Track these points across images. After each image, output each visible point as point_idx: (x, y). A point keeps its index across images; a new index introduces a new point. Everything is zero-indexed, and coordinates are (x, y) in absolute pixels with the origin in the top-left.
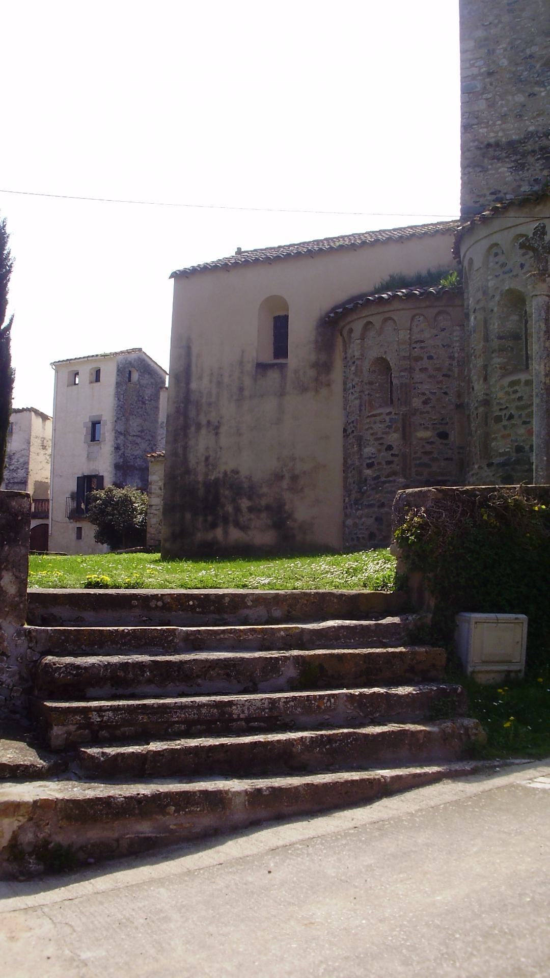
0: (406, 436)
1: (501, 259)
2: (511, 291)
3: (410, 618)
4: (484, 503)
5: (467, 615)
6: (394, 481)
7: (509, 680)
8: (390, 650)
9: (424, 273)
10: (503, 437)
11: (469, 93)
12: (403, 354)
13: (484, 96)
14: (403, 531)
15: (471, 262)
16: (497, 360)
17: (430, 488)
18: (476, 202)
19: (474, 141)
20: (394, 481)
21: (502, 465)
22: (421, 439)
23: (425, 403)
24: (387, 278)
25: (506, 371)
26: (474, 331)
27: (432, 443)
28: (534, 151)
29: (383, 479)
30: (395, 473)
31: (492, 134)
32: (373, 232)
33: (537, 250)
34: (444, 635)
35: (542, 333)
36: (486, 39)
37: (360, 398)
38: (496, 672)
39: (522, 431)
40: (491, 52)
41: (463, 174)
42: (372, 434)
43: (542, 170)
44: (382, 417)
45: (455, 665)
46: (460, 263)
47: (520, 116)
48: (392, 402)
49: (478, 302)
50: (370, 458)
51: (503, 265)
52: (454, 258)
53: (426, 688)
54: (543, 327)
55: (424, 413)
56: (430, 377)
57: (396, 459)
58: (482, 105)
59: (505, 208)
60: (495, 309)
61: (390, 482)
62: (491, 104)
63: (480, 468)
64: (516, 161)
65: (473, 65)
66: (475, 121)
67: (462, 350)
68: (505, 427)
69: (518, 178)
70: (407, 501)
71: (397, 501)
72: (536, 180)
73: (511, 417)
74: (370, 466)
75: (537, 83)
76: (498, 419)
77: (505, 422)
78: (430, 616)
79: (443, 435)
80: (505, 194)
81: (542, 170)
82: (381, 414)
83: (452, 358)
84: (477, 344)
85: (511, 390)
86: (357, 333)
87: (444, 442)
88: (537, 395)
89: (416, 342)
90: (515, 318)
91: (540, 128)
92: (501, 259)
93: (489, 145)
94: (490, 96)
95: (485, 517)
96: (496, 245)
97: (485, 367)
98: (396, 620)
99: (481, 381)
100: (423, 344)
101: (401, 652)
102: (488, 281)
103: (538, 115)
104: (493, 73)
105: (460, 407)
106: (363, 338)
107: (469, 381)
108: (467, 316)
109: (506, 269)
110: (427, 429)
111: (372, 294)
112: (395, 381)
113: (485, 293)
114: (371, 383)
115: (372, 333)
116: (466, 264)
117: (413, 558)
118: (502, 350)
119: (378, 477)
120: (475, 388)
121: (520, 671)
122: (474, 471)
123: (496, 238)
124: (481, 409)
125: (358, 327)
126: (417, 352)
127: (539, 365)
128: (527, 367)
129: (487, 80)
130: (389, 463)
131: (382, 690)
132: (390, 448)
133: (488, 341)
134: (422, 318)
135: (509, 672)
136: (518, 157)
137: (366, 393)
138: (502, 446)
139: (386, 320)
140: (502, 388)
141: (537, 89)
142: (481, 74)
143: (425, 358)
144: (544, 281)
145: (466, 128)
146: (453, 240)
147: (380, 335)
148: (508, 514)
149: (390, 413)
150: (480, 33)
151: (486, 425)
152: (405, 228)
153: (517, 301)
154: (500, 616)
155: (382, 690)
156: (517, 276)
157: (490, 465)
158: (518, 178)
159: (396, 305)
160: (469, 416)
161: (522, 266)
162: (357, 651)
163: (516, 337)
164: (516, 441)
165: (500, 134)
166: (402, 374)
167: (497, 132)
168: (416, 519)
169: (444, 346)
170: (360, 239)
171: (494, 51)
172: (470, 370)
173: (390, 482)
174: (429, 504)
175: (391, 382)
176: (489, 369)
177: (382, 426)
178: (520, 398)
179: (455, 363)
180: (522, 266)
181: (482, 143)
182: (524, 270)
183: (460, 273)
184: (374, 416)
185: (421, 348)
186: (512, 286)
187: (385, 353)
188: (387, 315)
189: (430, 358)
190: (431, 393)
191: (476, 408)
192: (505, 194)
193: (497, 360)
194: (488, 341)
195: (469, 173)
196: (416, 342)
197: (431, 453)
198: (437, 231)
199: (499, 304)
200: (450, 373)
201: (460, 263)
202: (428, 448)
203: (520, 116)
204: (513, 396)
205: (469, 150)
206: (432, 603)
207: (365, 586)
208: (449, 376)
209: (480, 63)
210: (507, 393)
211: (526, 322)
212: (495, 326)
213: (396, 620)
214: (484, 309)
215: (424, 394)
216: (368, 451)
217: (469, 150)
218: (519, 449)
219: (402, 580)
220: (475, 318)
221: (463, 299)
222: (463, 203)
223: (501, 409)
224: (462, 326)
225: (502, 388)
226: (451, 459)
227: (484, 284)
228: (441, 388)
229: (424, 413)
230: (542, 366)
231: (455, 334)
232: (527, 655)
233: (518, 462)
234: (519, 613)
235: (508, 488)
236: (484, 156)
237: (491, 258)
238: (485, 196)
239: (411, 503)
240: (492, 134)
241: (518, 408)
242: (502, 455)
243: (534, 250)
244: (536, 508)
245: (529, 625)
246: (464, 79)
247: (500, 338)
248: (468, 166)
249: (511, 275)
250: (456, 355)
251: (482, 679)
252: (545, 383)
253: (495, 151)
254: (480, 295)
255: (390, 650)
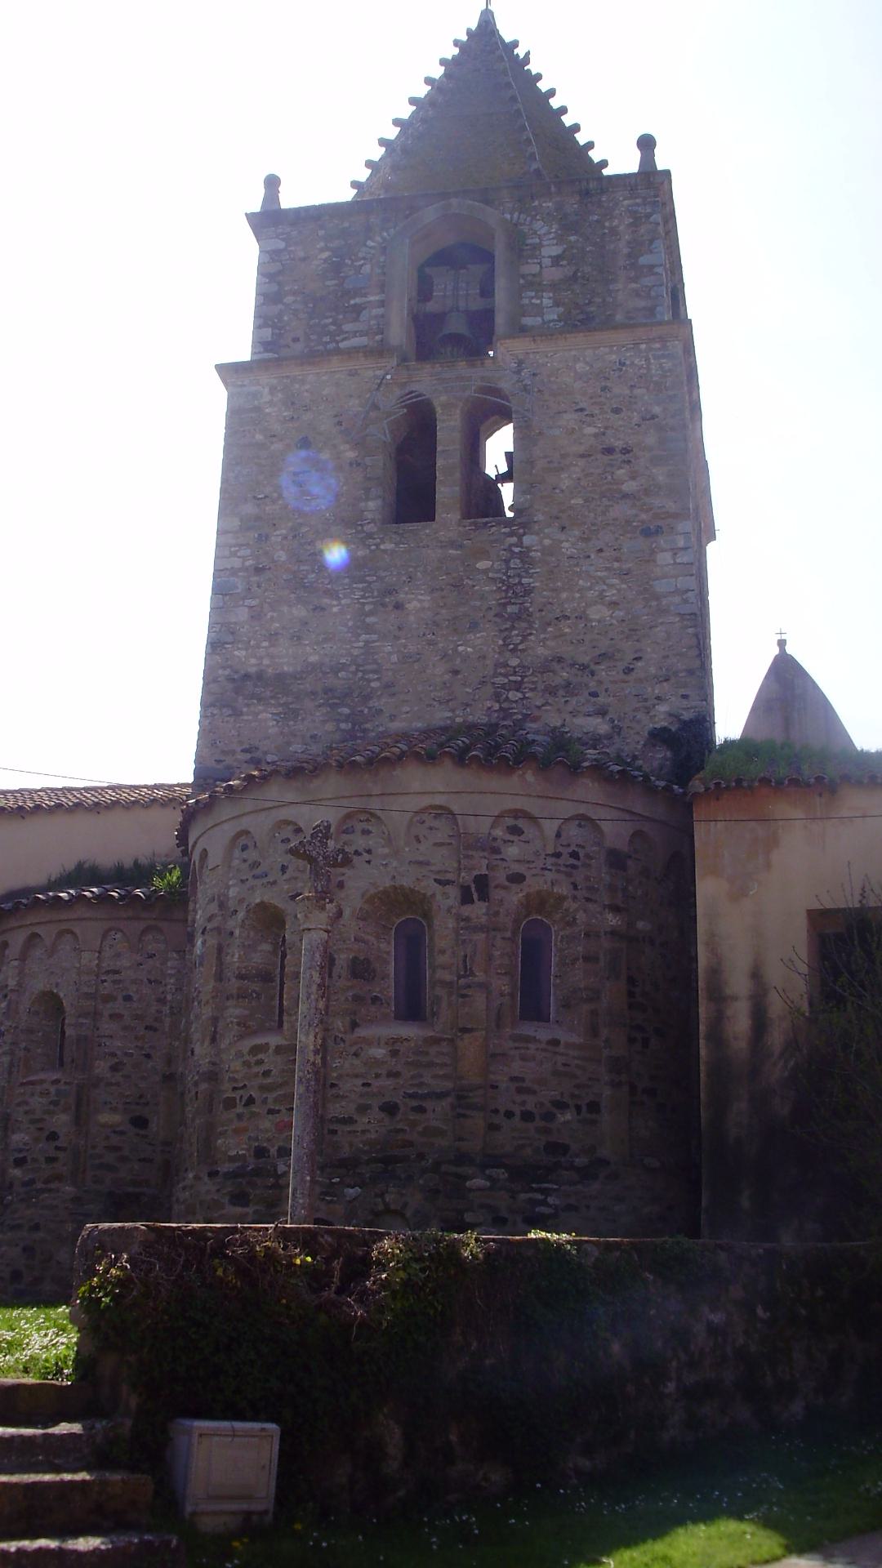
0: (79, 1120)
1: (252, 855)
2: (262, 906)
3: (98, 1425)
4: (219, 1250)
5: (187, 1422)
6: (58, 1190)
7: (249, 1526)
8: (67, 1477)
9: (128, 863)
10: (237, 1132)
11: (223, 592)
12: (86, 989)
13: (247, 602)
14: (92, 1289)
15: (204, 854)
16: (234, 1011)
17: (138, 1224)
18: (219, 761)
19: (224, 668)
20: (58, 1190)
21: (233, 1175)
22: (104, 1126)
23: (114, 1068)
24: (70, 866)
25: (246, 1029)
26: (201, 964)
27: (122, 1133)
28: (313, 693)
29: (39, 1185)
30: (59, 1178)
31: (253, 661)
32: (52, 790)
33: (315, 860)
34: (150, 1452)
35: (315, 987)
36: (258, 518)
37: (12, 1053)
38: (233, 1513)
39: (266, 1123)
40: (263, 538)
41: (203, 716)
42: (26, 1113)
43: (324, 722)
44: (46, 1086)
45: (167, 1502)
46: (185, 853)
47: (297, 638)
48: (62, 1064)
49: (210, 919)
50: (20, 1151)
51: (256, 865)
52: (178, 846)
53: (123, 1540)
54: (317, 978)
55: (111, 1084)
56: (125, 1028)
57: (61, 1155)
58: (242, 614)
59: (265, 778)
60: (237, 932)
61: (50, 1190)
62: (256, 616)
63: (197, 1178)
64: (286, 704)
65: (234, 554)
66: (230, 638)
67: (179, 989)
68: (240, 1117)
69: (286, 730)
70: (100, 1242)
71: (84, 1240)
72: (313, 737)
73: (251, 1101)
74: (20, 1163)
75: (327, 593)
76: (230, 1104)
77: (239, 1109)
78: (129, 1423)
79: (140, 1122)
80: (266, 753)
81: (324, 722)
82: (42, 1082)
83: (162, 1001)
84: (204, 982)
85: (253, 1060)
86: (14, 951)
87: (142, 1132)
88: (300, 1081)
89: (108, 972)
90: (266, 947)
91: (327, 660)
92: (252, 855)
93: (247, 676)
94: (254, 603)
95: (220, 1272)
96: (246, 833)
97: (215, 1020)
98: (76, 1428)
99: (207, 1043)
100: (117, 977)
101: (84, 1481)
102: (228, 887)
103: (326, 640)
104: (263, 569)
105: (169, 1078)
106: (23, 957)
107: (187, 1041)
108: (191, 938)
109: (258, 871)
110: (114, 1110)
111: (43, 890)
112: (69, 1032)
113: (222, 906)
114: (30, 1031)
115: (38, 952)
116: (196, 857)
117: (100, 1329)
118: (242, 995)
119: (32, 1182)
120: (197, 1051)
121: (266, 1512)
122: (188, 1182)
123: (245, 823)
124: (204, 1086)
125: (17, 939)
126: (107, 988)
127: (307, 1034)
128: (281, 1025)
129: (254, 579)
130: (51, 1160)
131: (53, 1544)
132: (53, 1136)
133: (221, 980)
134: (119, 936)
135: (248, 1514)
136: (290, 699)
137: (23, 1045)
138: (233, 1146)
139: (61, 934)
140: (239, 1054)
141: (326, 601)
142: (245, 569)
143: (120, 998)
144: (323, 908)
145: (215, 645)
146: (179, 818)
147: (50, 957)
148: (258, 1269)
149: (56, 1082)
150: (249, 509)
151: (211, 1111)
152: (102, 789)
153: (270, 921)
154: (238, 1425)
155: (53, 1544)
156: (275, 883)
157: (213, 1174)
158: (286, 730)
159: (81, 911)
160: (182, 1094)
161: (284, 869)
162: (15, 1478)
163: (265, 977)
164: (257, 1139)
165: (266, 662)
166: (81, 1020)
167: (261, 658)
168: (113, 1271)
169: (150, 982)
170: (32, 799)
171: (267, 537)
172: (189, 1023)
173: (50, 1190)
174: (136, 1248)
175: (63, 1033)
176: (221, 1024)
177: (44, 1100)
178: (266, 1074)
179: (166, 1009)
180: (284, 869)
181: (236, 672)
182: (286, 876)
183: (185, 869)
184: (32, 1083)
185: (114, 982)
186: (266, 899)
187: (57, 985)
188: (64, 926)
189: (128, 998)
190: (126, 1054)
191: (196, 1084)
192: (266, 753)
193: (234, 1011)
194: (221, 980)
195: (213, 715)
196: (108, 972)
197: (117, 1149)
198: (155, 800)
199: (242, 926)
200: (156, 1025)
201: (185, 853)
202: (115, 1140)
203: (297, 638)
204: (256, 1069)
205: (215, 681)
206: (133, 1401)
207: (26, 1370)
208: (155, 1030)
209: (246, 552)
210: (247, 1064)
211: (284, 956)
212: (234, 957)
213: (76, 1428)
214: (218, 930)
215: (114, 1055)
216: (18, 1138)
217: (215, 681)
218: (260, 1152)
219: (85, 1363)
220: (204, 943)
221: (186, 911)
222: (199, 760)
223: (235, 1089)
224: (181, 952)
225: (239, 1054)
226: (151, 1161)
227: (223, 888)
228: (142, 1048)
229: (111, 1084)
230: (311, 1037)
231: (169, 964)
232: (278, 1487)
233: (257, 1172)
234: (267, 1421)
235: (256, 1229)
236: (237, 691)
237: (237, 853)
238: (233, 752)
239: (106, 1244)
240: (253, 661)
241: (263, 1088)
242: (232, 1159)
243: (311, 860)
244: (298, 1262)
245: (282, 1439)
246: (218, 572)
247: (241, 977)
248: (212, 705)
249: (265, 880)
250: (169, 997)
251: (207, 1524)
252: (314, 1064)
253: (256, 686)
254: (214, 908)
255: (67, 1477)
